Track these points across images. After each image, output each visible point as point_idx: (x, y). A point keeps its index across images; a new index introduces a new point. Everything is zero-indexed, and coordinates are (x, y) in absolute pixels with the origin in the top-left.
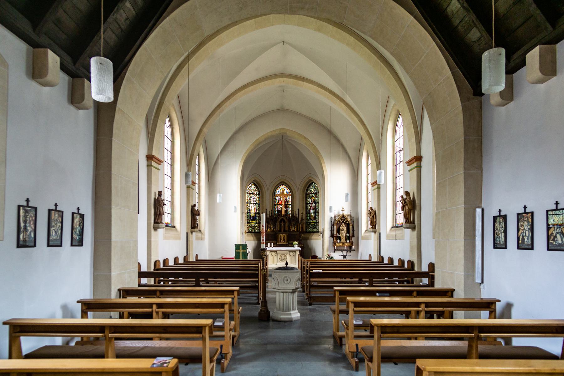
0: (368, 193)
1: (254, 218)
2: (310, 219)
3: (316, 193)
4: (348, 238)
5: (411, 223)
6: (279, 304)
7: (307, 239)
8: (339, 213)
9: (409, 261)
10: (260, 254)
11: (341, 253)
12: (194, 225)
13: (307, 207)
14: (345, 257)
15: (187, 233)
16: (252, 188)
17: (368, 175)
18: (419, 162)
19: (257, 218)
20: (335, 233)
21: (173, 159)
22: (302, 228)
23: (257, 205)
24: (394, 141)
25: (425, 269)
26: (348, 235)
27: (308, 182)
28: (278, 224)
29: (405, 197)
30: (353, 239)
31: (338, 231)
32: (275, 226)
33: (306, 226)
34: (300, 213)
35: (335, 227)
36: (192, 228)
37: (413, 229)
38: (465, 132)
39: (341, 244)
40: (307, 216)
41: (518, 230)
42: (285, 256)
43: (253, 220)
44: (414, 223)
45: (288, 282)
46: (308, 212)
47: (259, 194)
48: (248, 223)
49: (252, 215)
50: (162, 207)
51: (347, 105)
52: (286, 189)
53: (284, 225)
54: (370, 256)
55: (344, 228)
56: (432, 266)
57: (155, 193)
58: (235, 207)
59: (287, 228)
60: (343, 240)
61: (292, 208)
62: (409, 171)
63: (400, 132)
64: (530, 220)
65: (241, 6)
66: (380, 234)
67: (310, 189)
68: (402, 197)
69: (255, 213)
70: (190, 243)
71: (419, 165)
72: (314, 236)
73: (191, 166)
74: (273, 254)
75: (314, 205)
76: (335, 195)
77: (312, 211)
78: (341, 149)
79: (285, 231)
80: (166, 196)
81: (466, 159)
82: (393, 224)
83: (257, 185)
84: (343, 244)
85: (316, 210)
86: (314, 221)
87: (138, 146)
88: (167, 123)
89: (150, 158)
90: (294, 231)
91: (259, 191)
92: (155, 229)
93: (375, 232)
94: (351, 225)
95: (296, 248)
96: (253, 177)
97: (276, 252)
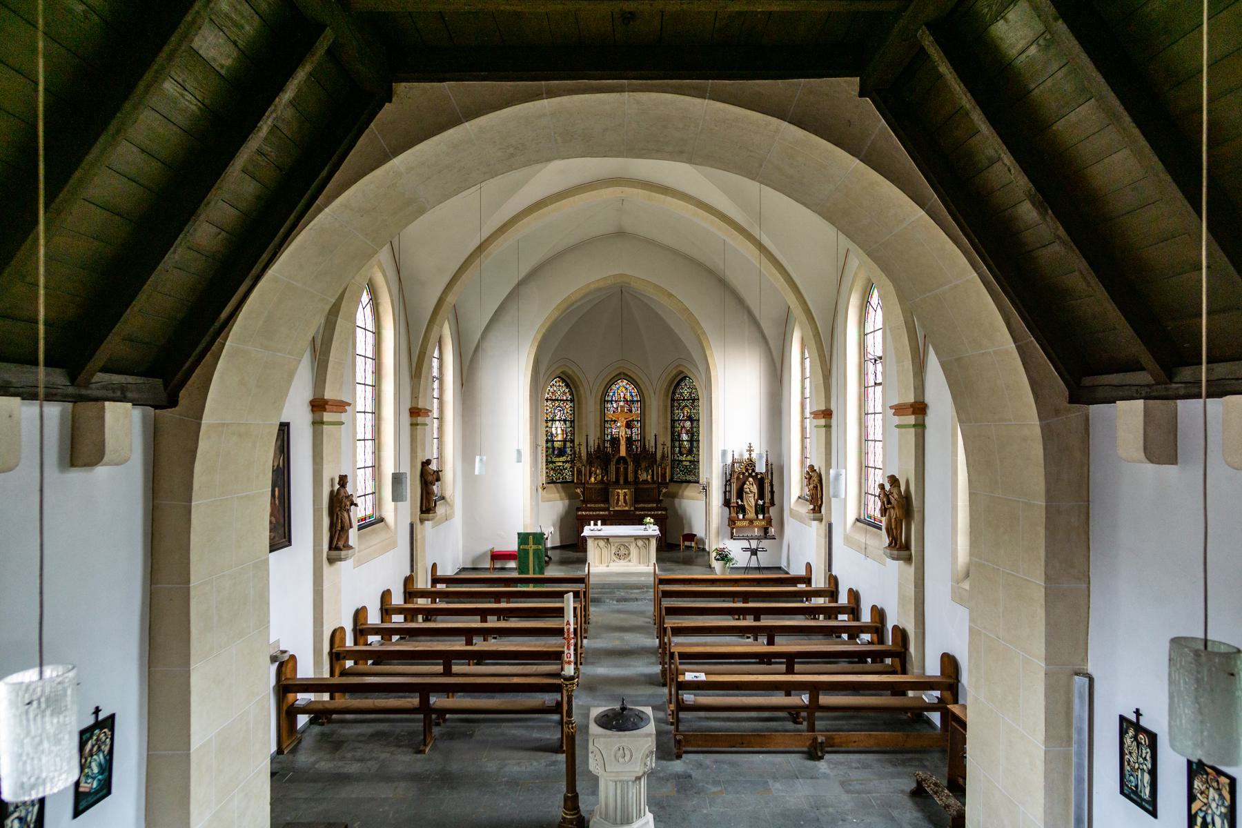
0: (803, 438)
1: (562, 452)
2: (681, 453)
3: (694, 400)
4: (761, 509)
5: (901, 549)
6: (607, 797)
7: (674, 496)
8: (741, 455)
9: (895, 628)
10: (574, 547)
11: (745, 544)
12: (428, 504)
13: (673, 427)
14: (754, 552)
15: (412, 526)
16: (560, 390)
17: (803, 379)
18: (920, 417)
19: (568, 451)
20: (734, 499)
21: (378, 372)
22: (664, 476)
23: (568, 424)
24: (863, 336)
25: (933, 668)
26: (760, 502)
27: (676, 376)
28: (613, 468)
29: (888, 487)
30: (773, 512)
31: (740, 494)
32: (606, 471)
33: (672, 468)
34: (660, 441)
35: (734, 487)
36: (422, 512)
37: (908, 560)
38: (1048, 491)
39: (745, 523)
40: (673, 447)
41: (1191, 798)
42: (627, 548)
43: (559, 456)
44: (907, 547)
45: (627, 758)
46: (675, 438)
47: (572, 401)
48: (547, 462)
49: (557, 445)
50: (348, 511)
51: (761, 247)
52: (630, 387)
53: (626, 469)
54: (809, 566)
55: (751, 487)
56: (950, 663)
57: (332, 480)
58: (519, 452)
59: (631, 477)
60: (751, 514)
61: (643, 428)
62: (897, 426)
63: (876, 319)
64: (1227, 797)
65: (511, 150)
66: (830, 526)
67: (683, 397)
68: (882, 487)
69: (565, 441)
70: (418, 545)
71: (920, 421)
72: (690, 491)
73: (420, 377)
74: (602, 543)
75: (688, 424)
76: (734, 422)
77: (685, 437)
78: (746, 317)
79: (626, 481)
80: (361, 485)
81: (1050, 555)
82: (860, 514)
83: (568, 381)
84: (751, 521)
85: (693, 435)
86: (689, 458)
87: (291, 375)
88: (365, 298)
89: (318, 405)
90: (646, 481)
91: (571, 394)
92: (331, 561)
93: (821, 520)
94: (767, 482)
95: (653, 530)
96: (560, 372)
97: (607, 539)
